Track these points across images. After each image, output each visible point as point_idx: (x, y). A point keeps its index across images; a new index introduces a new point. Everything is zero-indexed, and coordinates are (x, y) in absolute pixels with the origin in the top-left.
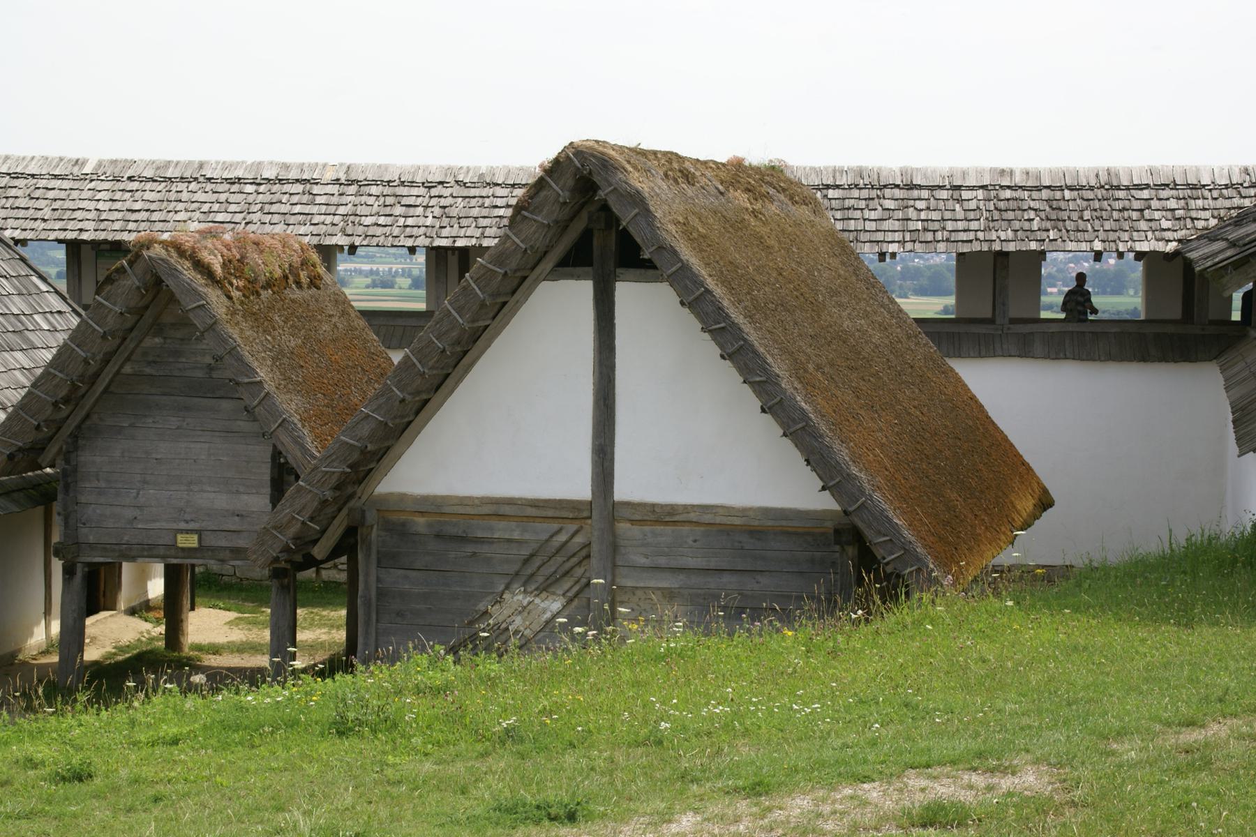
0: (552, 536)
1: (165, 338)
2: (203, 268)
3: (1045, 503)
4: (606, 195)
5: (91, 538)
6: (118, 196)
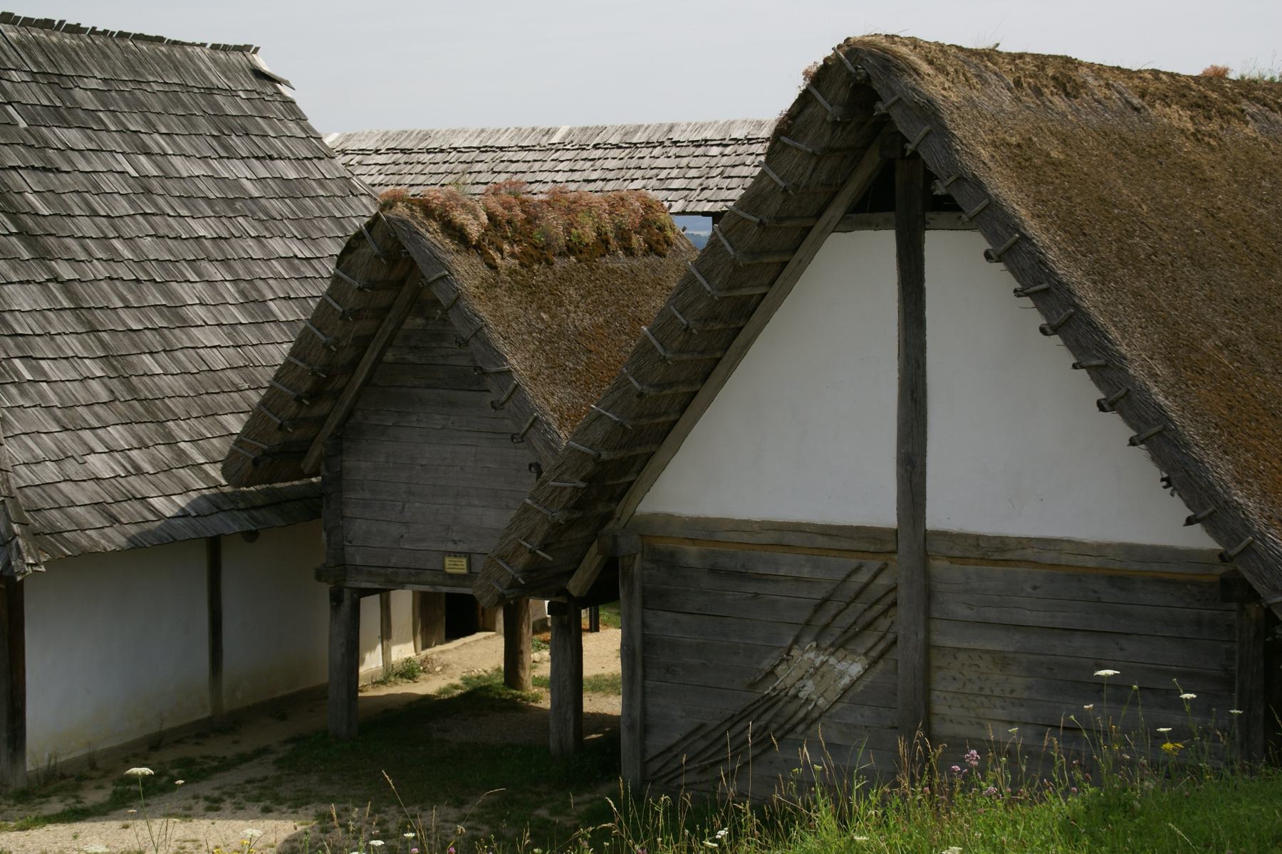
0: (849, 576)
1: (427, 318)
2: (456, 232)
4: (888, 108)
5: (358, 558)
6: (579, 166)
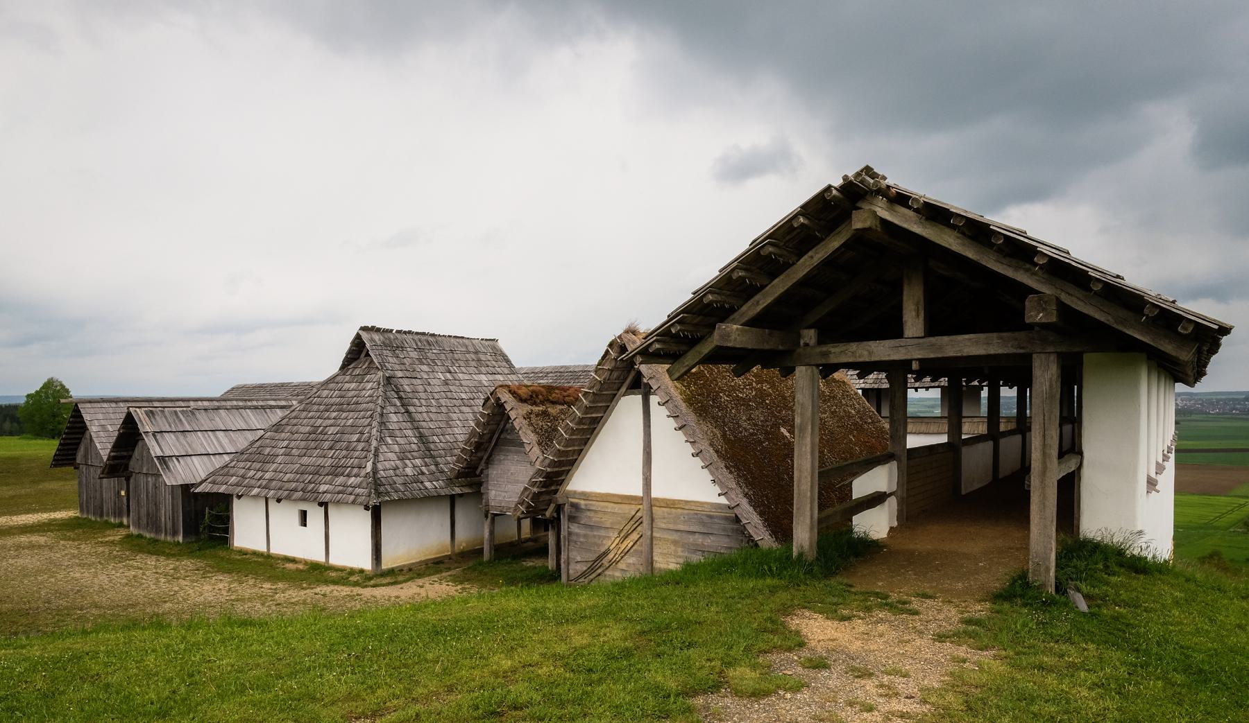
3: (868, 170)
